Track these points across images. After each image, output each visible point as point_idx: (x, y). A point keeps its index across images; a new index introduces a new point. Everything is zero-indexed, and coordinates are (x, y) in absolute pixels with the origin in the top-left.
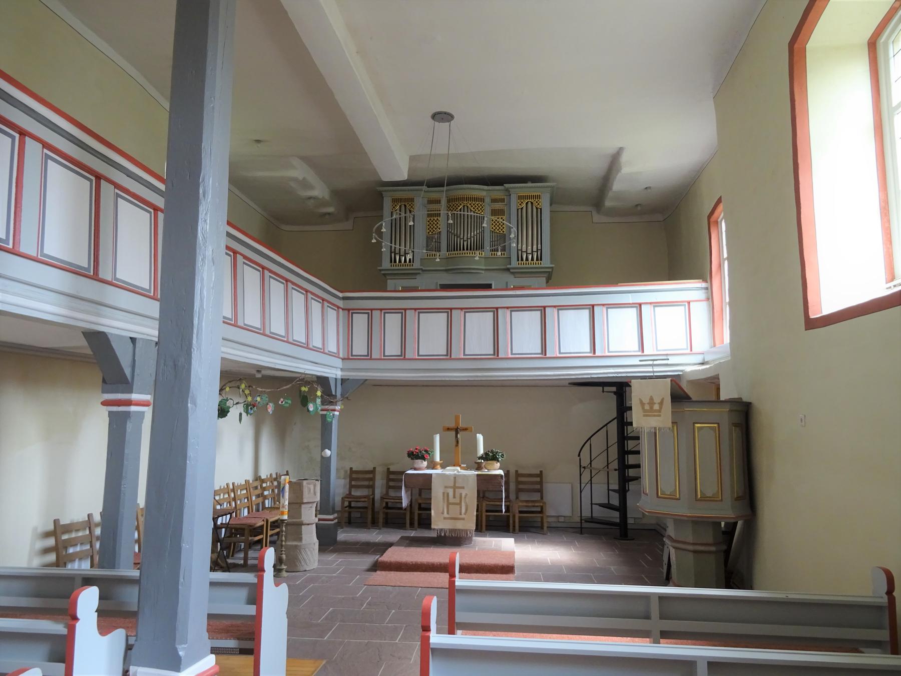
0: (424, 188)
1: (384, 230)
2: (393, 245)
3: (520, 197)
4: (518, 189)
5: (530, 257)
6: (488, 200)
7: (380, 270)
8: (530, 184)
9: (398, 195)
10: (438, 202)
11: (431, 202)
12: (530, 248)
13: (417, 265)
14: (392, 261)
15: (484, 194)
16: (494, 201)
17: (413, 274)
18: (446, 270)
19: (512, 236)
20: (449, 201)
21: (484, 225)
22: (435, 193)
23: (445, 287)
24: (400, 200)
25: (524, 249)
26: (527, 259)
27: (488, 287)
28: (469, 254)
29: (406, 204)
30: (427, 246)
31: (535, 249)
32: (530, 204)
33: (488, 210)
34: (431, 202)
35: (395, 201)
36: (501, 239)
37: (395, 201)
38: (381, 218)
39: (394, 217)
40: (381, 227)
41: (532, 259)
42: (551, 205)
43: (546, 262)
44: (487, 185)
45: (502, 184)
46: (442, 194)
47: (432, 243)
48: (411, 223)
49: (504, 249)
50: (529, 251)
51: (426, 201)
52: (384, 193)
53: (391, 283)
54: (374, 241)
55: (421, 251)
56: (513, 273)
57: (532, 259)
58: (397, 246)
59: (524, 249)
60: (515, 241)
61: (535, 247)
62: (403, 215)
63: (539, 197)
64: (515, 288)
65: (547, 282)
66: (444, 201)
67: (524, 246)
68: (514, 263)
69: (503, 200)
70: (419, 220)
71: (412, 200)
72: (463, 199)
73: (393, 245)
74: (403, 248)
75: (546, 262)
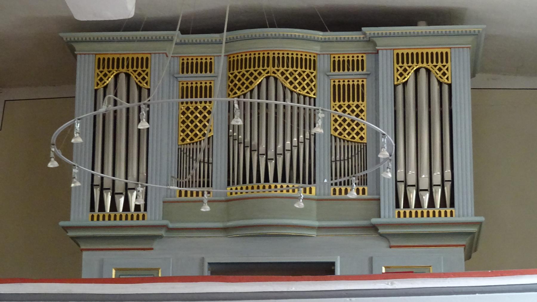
0: (177, 35)
1: (77, 139)
2: (98, 173)
3: (400, 58)
4: (394, 40)
5: (426, 198)
6: (324, 64)
7: (66, 229)
8: (422, 28)
9: (113, 50)
10: (206, 67)
11: (187, 67)
12: (424, 177)
13: (154, 216)
14: (95, 206)
15: (316, 48)
16: (338, 65)
17: (145, 239)
18: (226, 229)
19: (384, 154)
20: (232, 65)
21: (318, 130)
22: (199, 47)
23: (223, 271)
24: (118, 63)
25: (412, 180)
26: (419, 204)
27: (326, 270)
28: (282, 189)
29: (128, 74)
30: (179, 174)
31: (437, 180)
32: (423, 74)
33: (323, 90)
34: (187, 67)
35: (104, 64)
36: (355, 159)
37: (104, 64)
38: (67, 108)
39: (103, 109)
40: (70, 132)
41: (432, 204)
42: (473, 75)
43: (465, 211)
44: (323, 30)
45: (358, 28)
46: (217, 50)
47: (192, 170)
48: (144, 125)
49: (363, 181)
50: (424, 184)
51: (177, 66)
52: (78, 47)
53: (90, 261)
54: (53, 164)
55: (164, 184)
56: (383, 236)
57: (432, 204)
58: (108, 176)
59: (412, 180)
60: (391, 165)
61: (437, 175)
62: (123, 105)
63: (444, 57)
64: (391, 274)
65: (468, 257)
66: (221, 66)
67: (412, 172)
68: (389, 214)
69: (358, 65)
70: (161, 120)
71: (145, 63)
72: (264, 61)
73: (98, 173)
74: (120, 179)
75: (465, 211)
